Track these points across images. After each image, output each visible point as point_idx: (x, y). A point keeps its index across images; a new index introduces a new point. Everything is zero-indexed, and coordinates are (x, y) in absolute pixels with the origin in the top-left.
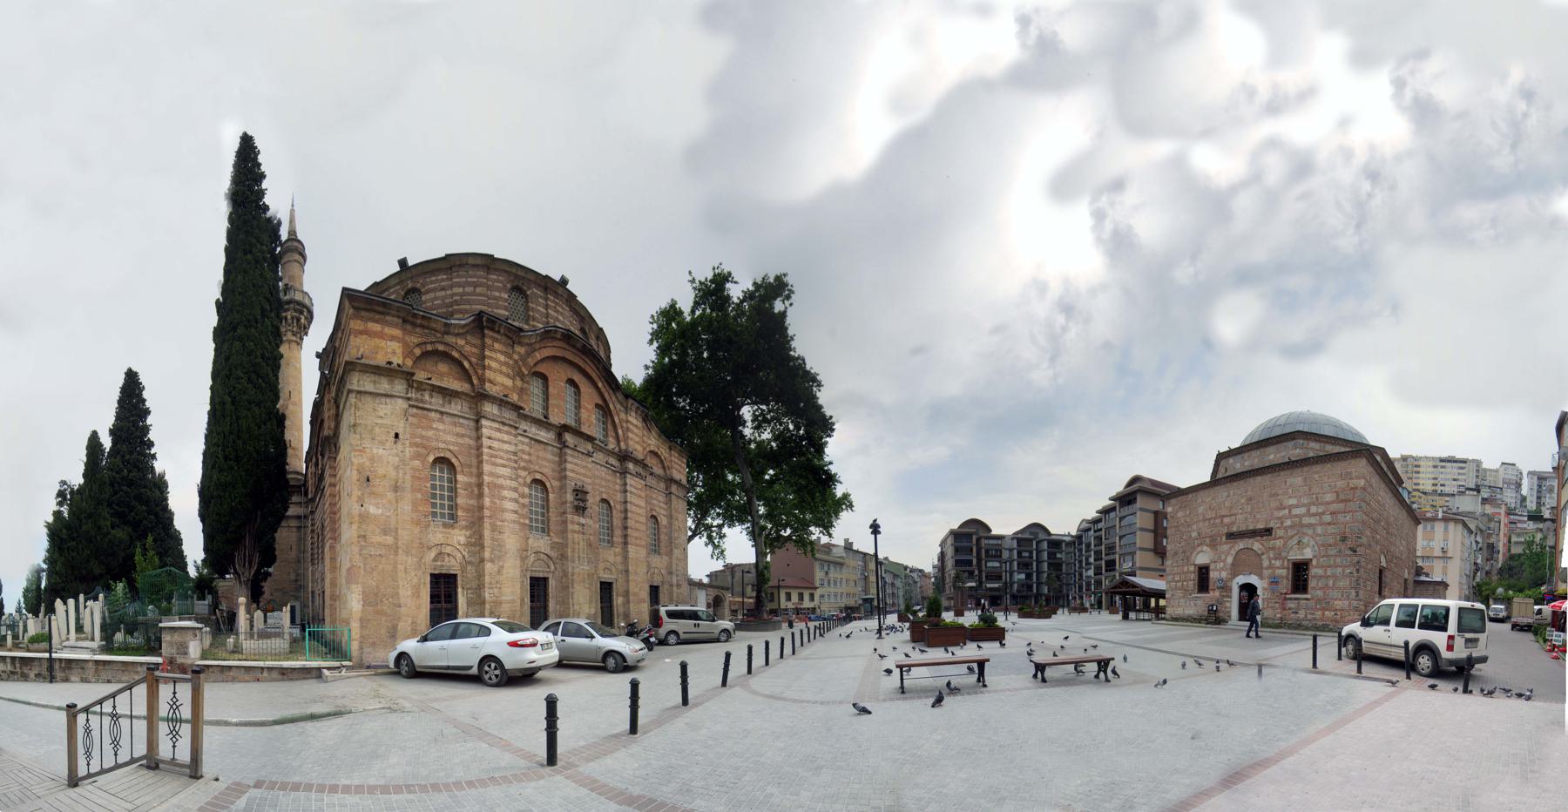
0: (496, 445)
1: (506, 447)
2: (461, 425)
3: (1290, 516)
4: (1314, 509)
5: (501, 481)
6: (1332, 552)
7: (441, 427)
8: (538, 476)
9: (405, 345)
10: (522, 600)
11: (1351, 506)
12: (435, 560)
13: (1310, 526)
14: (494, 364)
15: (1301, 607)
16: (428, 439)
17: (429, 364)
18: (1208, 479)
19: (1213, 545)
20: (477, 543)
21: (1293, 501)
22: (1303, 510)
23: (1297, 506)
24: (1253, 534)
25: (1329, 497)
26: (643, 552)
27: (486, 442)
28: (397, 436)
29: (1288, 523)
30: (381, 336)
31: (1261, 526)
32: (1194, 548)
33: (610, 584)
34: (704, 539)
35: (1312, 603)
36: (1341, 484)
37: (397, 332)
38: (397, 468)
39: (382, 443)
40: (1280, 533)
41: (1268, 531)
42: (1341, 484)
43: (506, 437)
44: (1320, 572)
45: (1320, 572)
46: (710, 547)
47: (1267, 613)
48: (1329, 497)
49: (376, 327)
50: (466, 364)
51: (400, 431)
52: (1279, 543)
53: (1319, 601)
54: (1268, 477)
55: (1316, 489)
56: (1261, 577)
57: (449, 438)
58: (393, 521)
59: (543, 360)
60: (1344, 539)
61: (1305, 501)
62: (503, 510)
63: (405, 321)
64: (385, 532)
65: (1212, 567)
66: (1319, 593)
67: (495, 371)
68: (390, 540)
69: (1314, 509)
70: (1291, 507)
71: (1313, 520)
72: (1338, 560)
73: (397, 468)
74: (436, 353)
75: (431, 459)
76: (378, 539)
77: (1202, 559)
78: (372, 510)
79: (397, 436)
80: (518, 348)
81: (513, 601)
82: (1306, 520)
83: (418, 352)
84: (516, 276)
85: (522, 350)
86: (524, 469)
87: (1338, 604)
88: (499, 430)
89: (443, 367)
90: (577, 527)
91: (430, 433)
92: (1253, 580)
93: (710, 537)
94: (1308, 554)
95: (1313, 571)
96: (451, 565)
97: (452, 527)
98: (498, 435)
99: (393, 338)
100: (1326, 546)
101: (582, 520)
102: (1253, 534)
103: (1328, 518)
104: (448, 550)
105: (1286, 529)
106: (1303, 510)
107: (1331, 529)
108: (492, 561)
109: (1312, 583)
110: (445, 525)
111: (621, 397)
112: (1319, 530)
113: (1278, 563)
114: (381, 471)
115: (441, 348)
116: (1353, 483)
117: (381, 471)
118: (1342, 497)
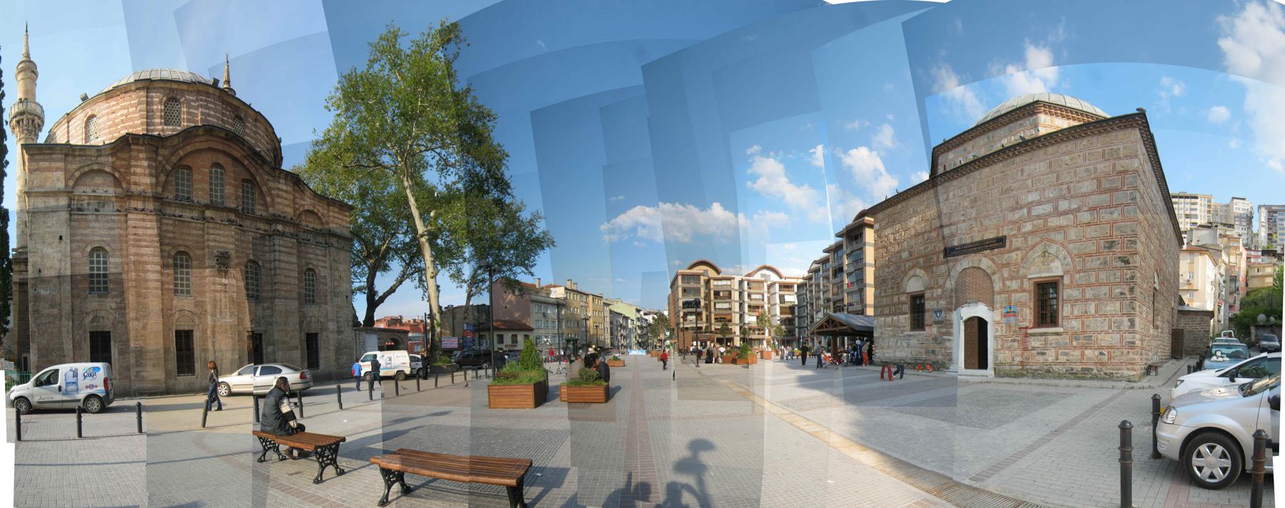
0: (140, 231)
1: (149, 232)
2: (113, 221)
3: (1030, 218)
4: (1063, 205)
5: (145, 259)
6: (1094, 263)
7: (96, 225)
8: (182, 249)
9: (66, 170)
10: (166, 350)
11: (1120, 197)
12: (92, 321)
13: (1059, 229)
14: (138, 170)
15: (1051, 347)
16: (86, 235)
17: (87, 180)
18: (925, 176)
19: (928, 267)
20: (122, 309)
21: (1033, 197)
22: (1048, 208)
23: (1039, 203)
24: (981, 246)
25: (1087, 186)
26: (294, 305)
27: (131, 231)
28: (61, 238)
29: (1028, 227)
30: (49, 169)
31: (990, 235)
32: (905, 273)
33: (260, 335)
34: (416, 282)
35: (1065, 339)
36: (1103, 167)
37: (61, 165)
38: (60, 261)
39: (50, 244)
40: (1017, 242)
41: (1000, 242)
42: (1103, 167)
43: (149, 224)
44: (1076, 293)
45: (1076, 293)
46: (421, 290)
47: (1005, 356)
48: (1087, 186)
49: (46, 164)
50: (117, 175)
51: (63, 234)
52: (1015, 256)
53: (1075, 336)
54: (997, 168)
55: (1066, 177)
56: (991, 305)
57: (103, 232)
58: (57, 299)
59: (186, 155)
60: (1111, 245)
61: (1050, 194)
62: (146, 281)
63: (66, 155)
64: (52, 306)
65: (927, 295)
66: (1076, 324)
67: (140, 175)
68: (55, 311)
69: (1063, 205)
70: (1030, 206)
71: (1062, 221)
72: (1103, 276)
73: (60, 261)
74: (92, 171)
75: (89, 249)
76: (46, 311)
77: (913, 286)
78: (43, 292)
79: (61, 238)
80: (161, 151)
81: (158, 351)
82: (1054, 222)
83: (77, 174)
84: (171, 90)
85: (166, 152)
86: (169, 244)
87: (1106, 340)
88: (143, 220)
89: (99, 180)
90: (218, 287)
91: (87, 231)
92: (981, 311)
93: (421, 280)
94: (1056, 269)
95: (1066, 293)
96: (106, 325)
97: (105, 296)
98: (143, 224)
99: (58, 169)
100: (1084, 256)
101: (224, 281)
102: (981, 246)
103: (1085, 217)
104: (103, 313)
105: (1025, 236)
106: (1048, 208)
107: (1091, 232)
108: (137, 319)
109: (1065, 310)
110: (99, 296)
111: (267, 169)
112: (1073, 234)
113: (1014, 285)
114: (48, 265)
115: (95, 167)
116: (1120, 165)
117: (48, 265)
118: (1106, 185)
